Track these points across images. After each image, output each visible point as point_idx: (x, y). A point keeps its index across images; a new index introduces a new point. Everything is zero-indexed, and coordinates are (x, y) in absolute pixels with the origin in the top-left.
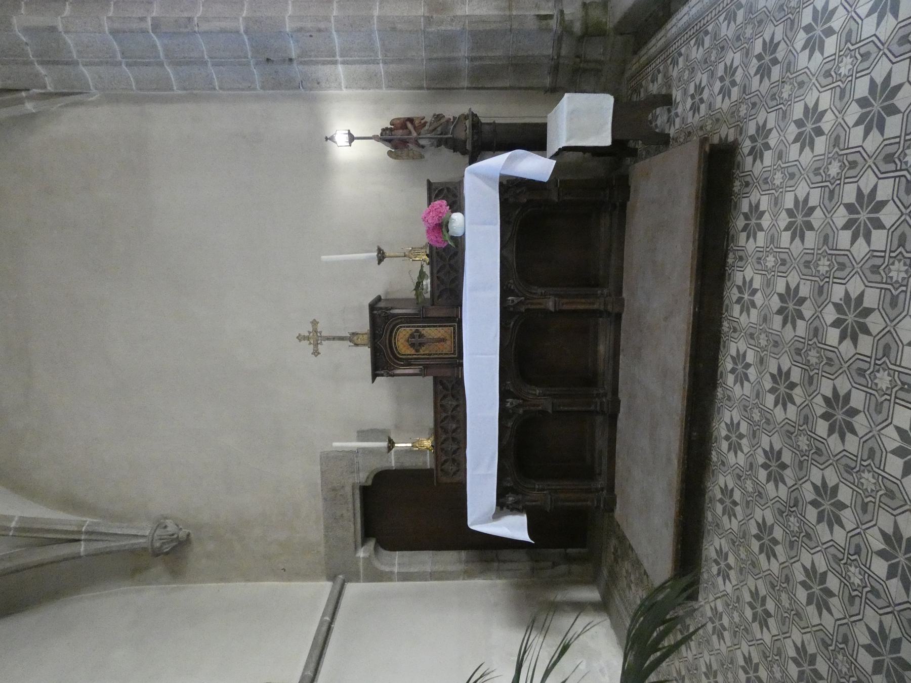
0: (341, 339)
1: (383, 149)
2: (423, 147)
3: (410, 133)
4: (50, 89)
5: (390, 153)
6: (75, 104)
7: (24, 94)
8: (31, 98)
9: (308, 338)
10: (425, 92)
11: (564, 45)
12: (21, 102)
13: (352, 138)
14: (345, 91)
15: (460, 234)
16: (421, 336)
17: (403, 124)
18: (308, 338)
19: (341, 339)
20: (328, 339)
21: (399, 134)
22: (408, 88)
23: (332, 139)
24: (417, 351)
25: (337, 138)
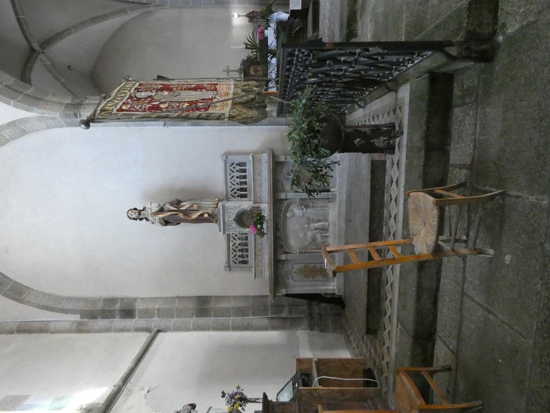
0: (235, 71)
1: (247, 19)
2: (258, 19)
3: (254, 14)
4: (157, 4)
5: (249, 21)
6: (162, 9)
7: (151, 5)
8: (152, 6)
9: (226, 71)
10: (258, 5)
11: (366, 59)
12: (150, 7)
13: (239, 16)
14: (236, 5)
15: (267, 36)
16: (257, 69)
17: (252, 12)
18: (226, 71)
19: (235, 71)
20: (231, 71)
21: (252, 15)
22: (254, 4)
23: (233, 16)
24: (256, 68)
25: (235, 16)
